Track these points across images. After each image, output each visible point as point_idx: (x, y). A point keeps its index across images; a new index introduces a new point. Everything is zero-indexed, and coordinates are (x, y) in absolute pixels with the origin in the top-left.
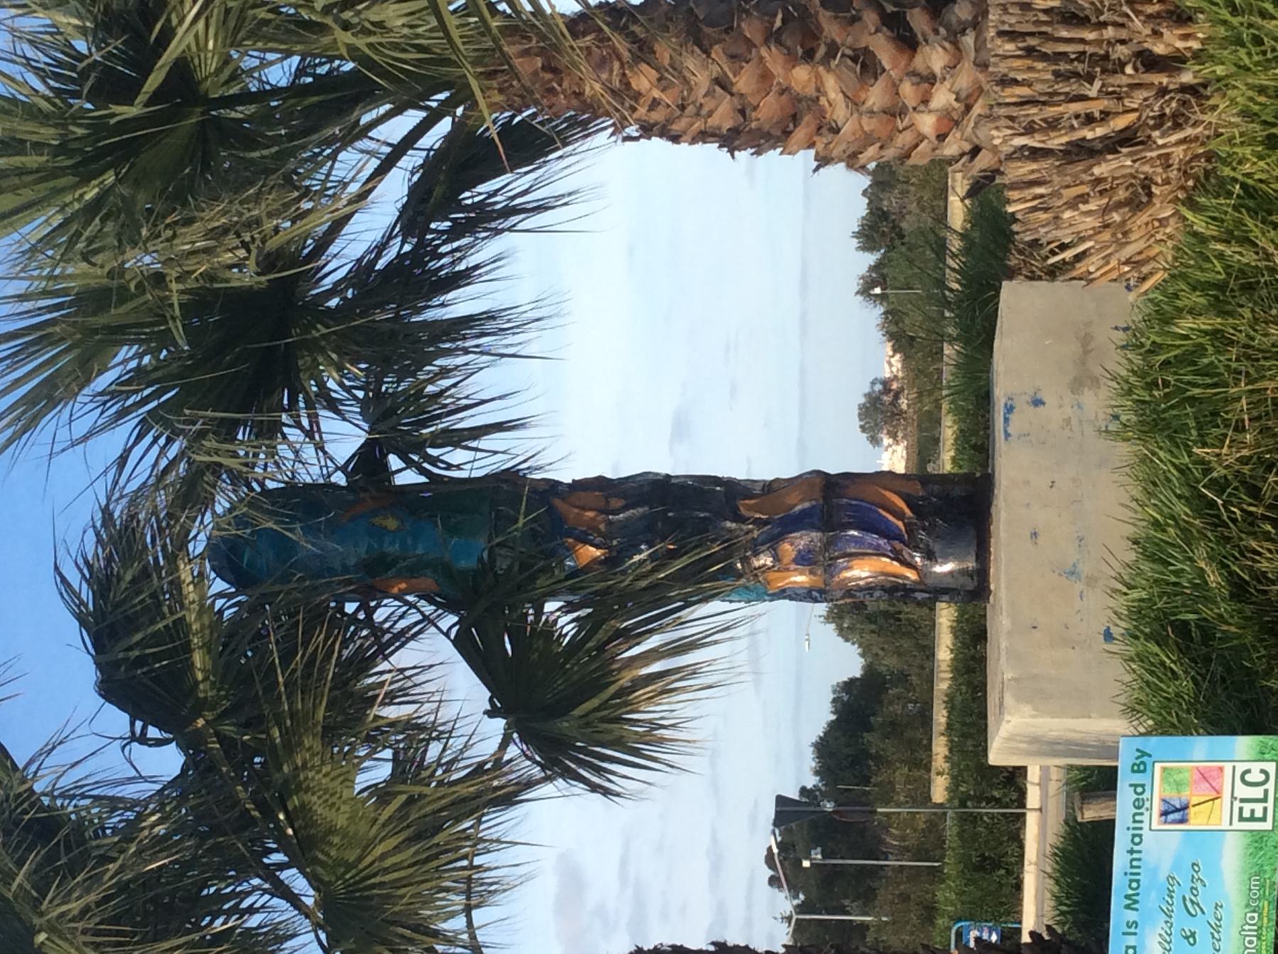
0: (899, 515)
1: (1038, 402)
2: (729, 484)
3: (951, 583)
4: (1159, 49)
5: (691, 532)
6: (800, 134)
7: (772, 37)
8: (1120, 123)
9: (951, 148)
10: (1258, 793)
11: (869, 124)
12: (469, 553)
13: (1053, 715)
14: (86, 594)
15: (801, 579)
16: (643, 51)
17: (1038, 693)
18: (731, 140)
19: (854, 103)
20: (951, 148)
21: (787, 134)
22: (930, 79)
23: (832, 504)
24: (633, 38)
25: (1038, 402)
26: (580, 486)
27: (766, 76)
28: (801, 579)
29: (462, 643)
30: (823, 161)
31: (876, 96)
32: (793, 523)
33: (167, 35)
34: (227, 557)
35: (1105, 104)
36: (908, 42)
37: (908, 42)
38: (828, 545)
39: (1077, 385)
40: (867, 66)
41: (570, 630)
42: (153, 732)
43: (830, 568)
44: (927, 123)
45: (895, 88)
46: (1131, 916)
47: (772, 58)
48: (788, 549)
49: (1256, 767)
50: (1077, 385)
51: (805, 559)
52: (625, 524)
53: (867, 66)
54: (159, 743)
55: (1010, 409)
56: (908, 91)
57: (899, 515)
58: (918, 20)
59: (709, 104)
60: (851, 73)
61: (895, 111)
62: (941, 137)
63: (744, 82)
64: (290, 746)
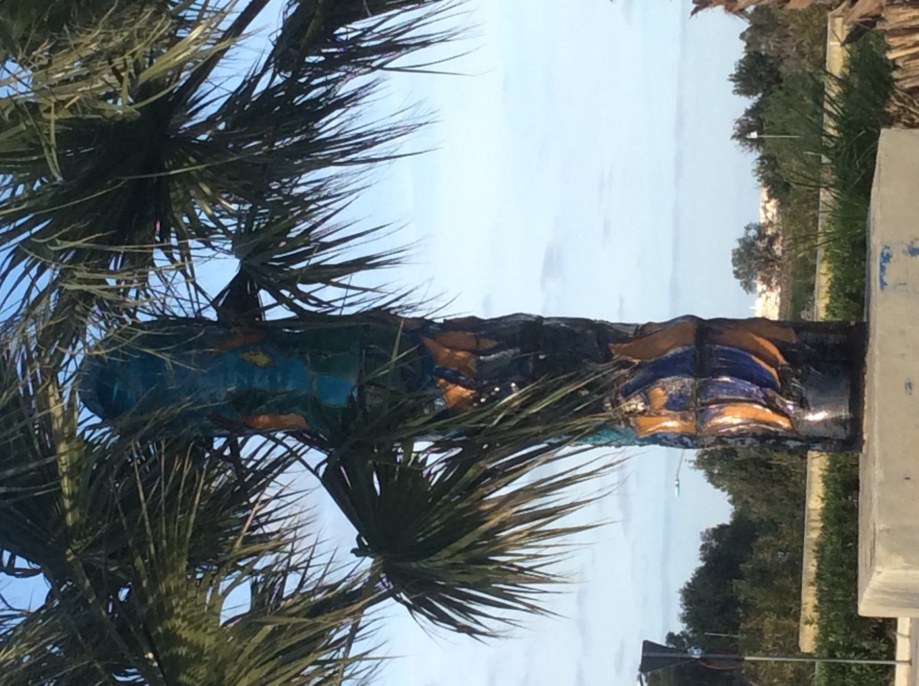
0: (773, 363)
3: (822, 431)
5: (566, 373)
12: (341, 389)
28: (672, 424)
32: (663, 368)
43: (702, 414)
48: (659, 394)
51: (676, 404)
55: (886, 258)
57: (773, 363)
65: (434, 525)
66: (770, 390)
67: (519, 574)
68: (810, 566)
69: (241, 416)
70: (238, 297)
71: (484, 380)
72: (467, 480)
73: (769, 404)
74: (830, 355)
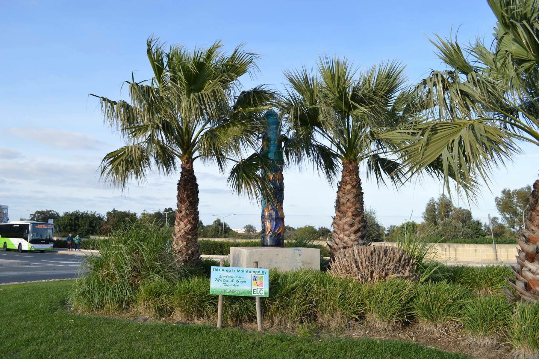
0: (278, 231)
1: (300, 255)
2: (282, 201)
3: (265, 240)
4: (374, 274)
5: (274, 195)
6: (339, 214)
7: (356, 209)
8: (361, 268)
9: (337, 240)
10: (258, 292)
11: (341, 226)
12: (271, 156)
13: (247, 258)
14: (260, 89)
15: (266, 214)
16: (354, 187)
17: (250, 255)
18: (338, 202)
19: (345, 223)
20: (337, 240)
21: (339, 211)
22: (349, 236)
23: (279, 219)
24: (356, 185)
25: (300, 255)
26: (282, 175)
27: (349, 208)
28: (266, 214)
29: (255, 154)
30: (334, 218)
31: (346, 227)
32: (276, 212)
33: (362, 106)
34: (270, 114)
35: (364, 265)
36: (355, 232)
37: (355, 232)
38: (273, 219)
39: (303, 262)
40: (352, 225)
41: (258, 174)
42: (236, 100)
43: (269, 219)
44: (341, 236)
45: (348, 230)
46: (236, 271)
47: (353, 209)
48: (272, 211)
49: (263, 292)
50: (303, 262)
51: (270, 215)
52: (276, 183)
53: (352, 225)
54: (234, 102)
55: (299, 250)
56: (348, 232)
57: (278, 231)
58: (359, 234)
59: (345, 198)
60: (350, 223)
61: (343, 230)
62: (339, 238)
63: (349, 204)
64: (242, 124)
65: (160, 139)
66: (273, 231)
67: (239, 187)
68: (205, 239)
69: (265, 139)
70: (285, 139)
71: (273, 182)
72: (256, 178)
73: (271, 231)
74: (278, 242)
